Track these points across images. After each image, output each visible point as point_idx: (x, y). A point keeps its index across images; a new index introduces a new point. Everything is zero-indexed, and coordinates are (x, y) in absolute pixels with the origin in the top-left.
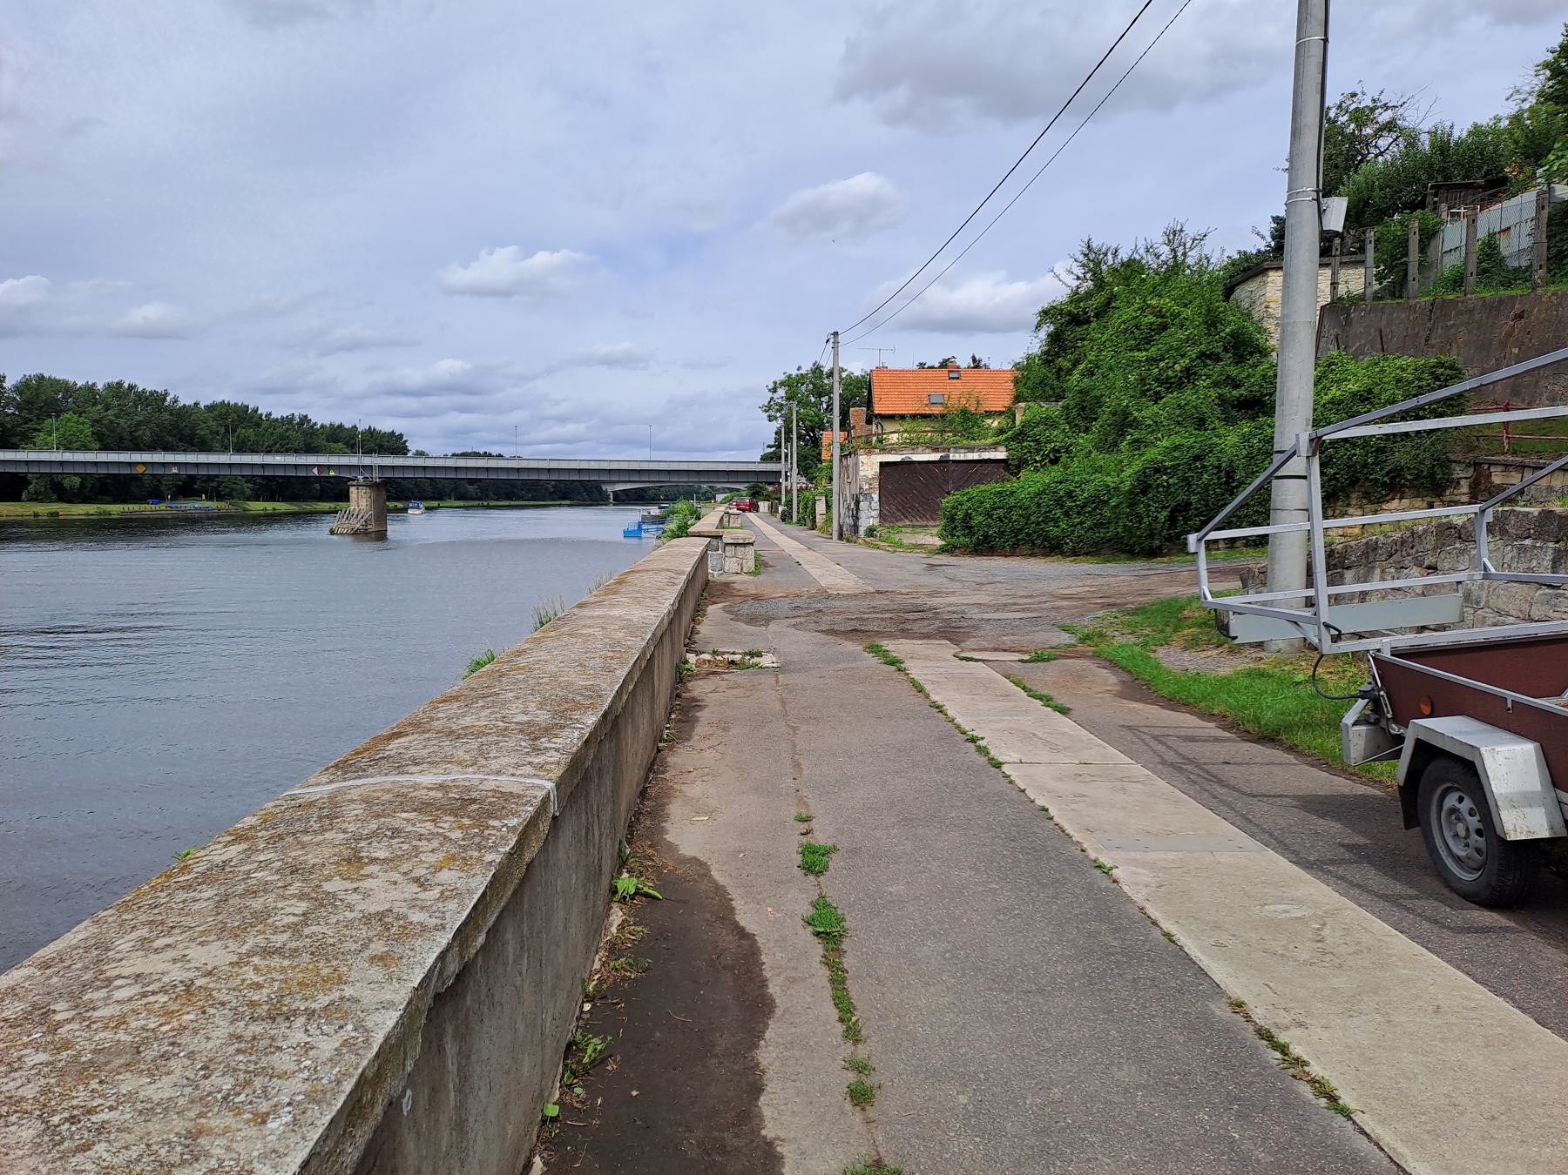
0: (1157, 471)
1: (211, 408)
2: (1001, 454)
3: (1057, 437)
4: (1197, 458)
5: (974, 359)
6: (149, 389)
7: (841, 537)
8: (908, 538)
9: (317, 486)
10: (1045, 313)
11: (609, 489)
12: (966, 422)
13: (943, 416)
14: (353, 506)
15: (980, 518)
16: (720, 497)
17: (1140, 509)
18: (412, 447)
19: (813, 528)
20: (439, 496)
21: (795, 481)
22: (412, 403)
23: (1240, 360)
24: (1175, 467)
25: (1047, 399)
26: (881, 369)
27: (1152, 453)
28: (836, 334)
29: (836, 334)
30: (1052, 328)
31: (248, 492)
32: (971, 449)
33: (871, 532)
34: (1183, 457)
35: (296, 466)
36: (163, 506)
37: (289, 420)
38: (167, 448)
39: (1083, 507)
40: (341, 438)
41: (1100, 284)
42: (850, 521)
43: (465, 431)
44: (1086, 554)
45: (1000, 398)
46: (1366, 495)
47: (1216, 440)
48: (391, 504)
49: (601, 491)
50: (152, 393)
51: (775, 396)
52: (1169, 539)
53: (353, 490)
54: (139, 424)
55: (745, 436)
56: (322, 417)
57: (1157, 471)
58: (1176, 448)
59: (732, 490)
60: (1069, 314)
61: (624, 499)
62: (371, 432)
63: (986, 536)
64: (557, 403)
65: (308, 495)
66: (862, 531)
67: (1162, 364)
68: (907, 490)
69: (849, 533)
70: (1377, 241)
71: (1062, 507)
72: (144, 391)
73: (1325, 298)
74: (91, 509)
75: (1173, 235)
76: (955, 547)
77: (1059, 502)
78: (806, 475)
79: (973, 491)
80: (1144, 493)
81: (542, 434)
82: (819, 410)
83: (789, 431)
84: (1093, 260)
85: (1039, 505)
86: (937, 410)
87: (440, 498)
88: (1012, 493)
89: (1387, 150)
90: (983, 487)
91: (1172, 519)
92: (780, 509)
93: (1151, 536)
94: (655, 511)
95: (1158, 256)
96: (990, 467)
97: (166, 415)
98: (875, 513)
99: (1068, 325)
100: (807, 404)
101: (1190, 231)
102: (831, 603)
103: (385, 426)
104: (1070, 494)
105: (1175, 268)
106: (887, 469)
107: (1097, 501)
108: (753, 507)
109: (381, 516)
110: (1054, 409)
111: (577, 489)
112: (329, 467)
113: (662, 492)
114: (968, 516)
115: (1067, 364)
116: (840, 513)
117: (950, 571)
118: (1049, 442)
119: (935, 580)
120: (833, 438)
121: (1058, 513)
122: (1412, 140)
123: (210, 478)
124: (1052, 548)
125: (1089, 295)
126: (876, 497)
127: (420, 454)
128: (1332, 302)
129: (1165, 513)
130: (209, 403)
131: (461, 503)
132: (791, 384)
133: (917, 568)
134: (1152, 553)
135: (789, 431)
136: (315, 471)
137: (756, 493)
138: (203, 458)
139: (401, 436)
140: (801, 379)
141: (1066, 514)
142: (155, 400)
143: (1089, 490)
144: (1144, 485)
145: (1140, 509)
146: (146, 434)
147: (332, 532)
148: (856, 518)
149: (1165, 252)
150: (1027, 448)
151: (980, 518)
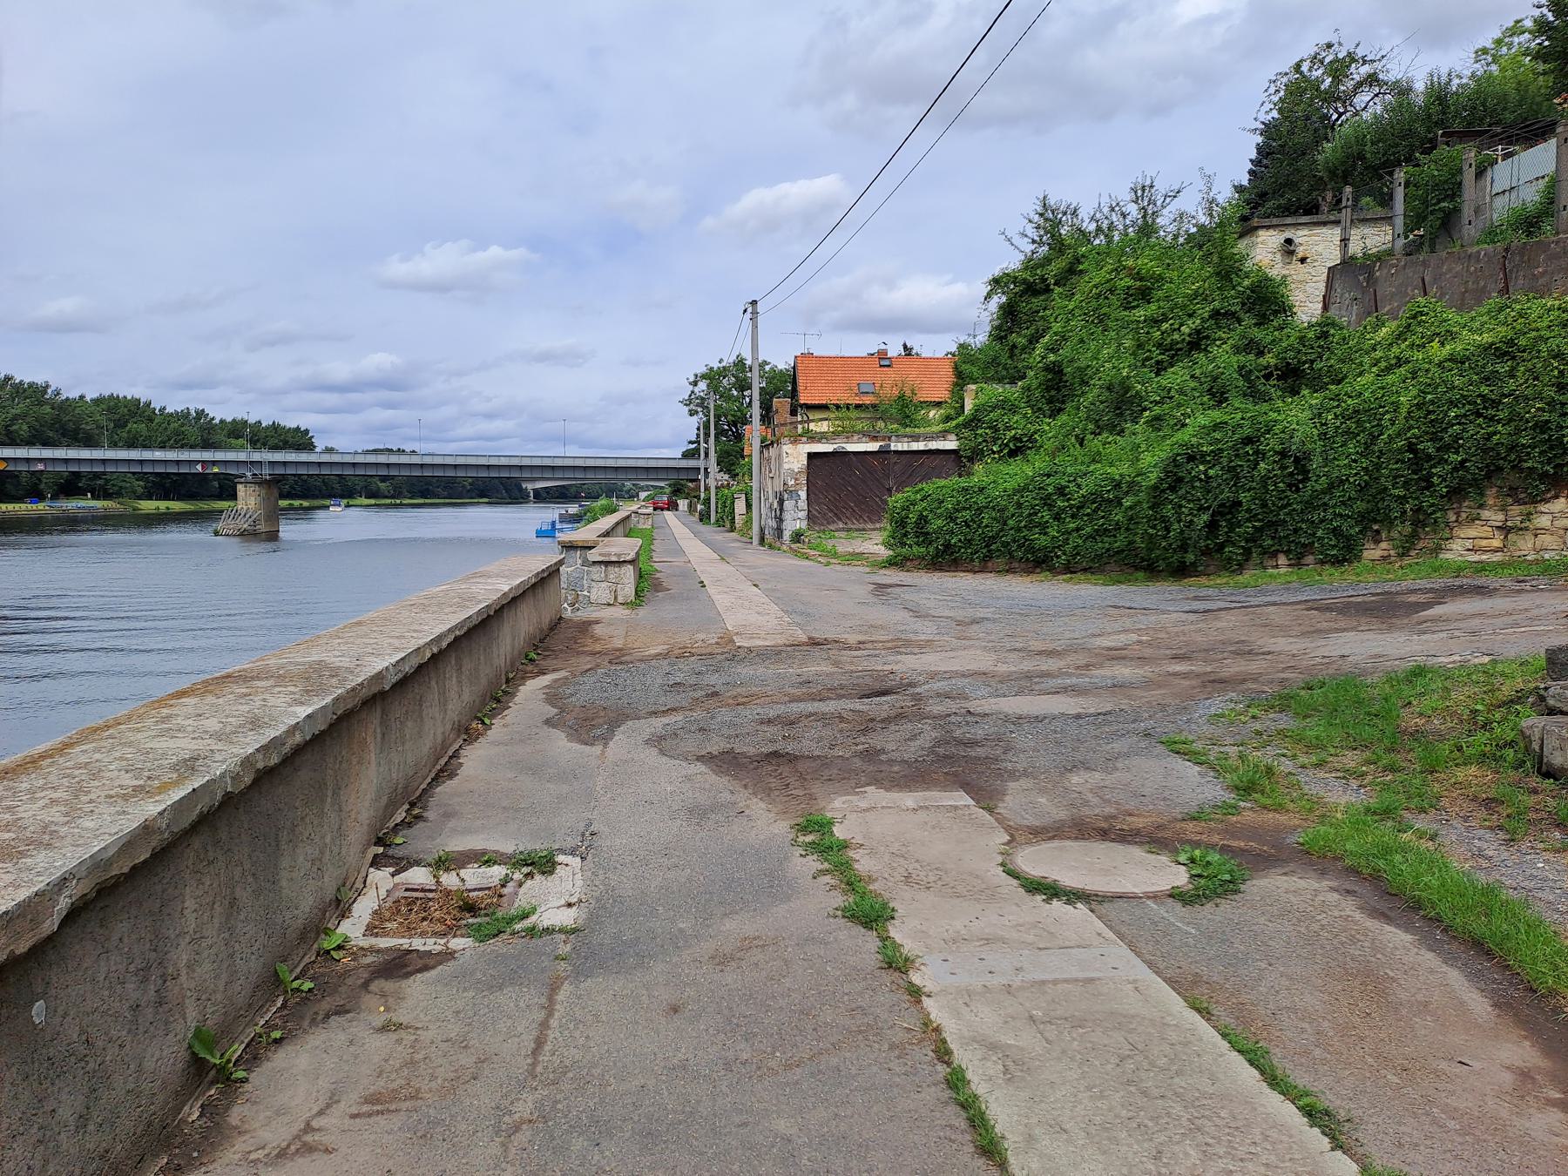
0: (1191, 458)
1: (97, 401)
2: (951, 444)
3: (1018, 424)
4: (1248, 441)
5: (905, 346)
6: (27, 380)
7: (762, 541)
8: (844, 545)
9: (216, 484)
10: (996, 281)
11: (529, 486)
12: (905, 411)
13: (874, 406)
14: (240, 504)
15: (939, 522)
16: (643, 495)
17: (1168, 511)
18: (320, 444)
19: (732, 530)
21: (716, 477)
22: (332, 399)
23: (1262, 321)
24: (1217, 454)
25: (1000, 380)
26: (808, 356)
27: (1183, 436)
28: (754, 303)
29: (754, 303)
30: (1004, 299)
31: (140, 490)
32: (916, 438)
33: (797, 537)
34: (1226, 439)
35: (178, 462)
36: (41, 506)
37: (185, 415)
38: (46, 443)
39: (1079, 508)
40: (237, 431)
41: (1058, 246)
42: (773, 523)
43: (389, 427)
44: (1085, 570)
45: (938, 388)
46: (1512, 492)
47: (1274, 415)
48: (283, 503)
49: (521, 489)
50: (31, 385)
51: (696, 390)
52: (1206, 552)
53: (239, 487)
54: (15, 418)
55: (668, 433)
56: (221, 412)
57: (1191, 458)
58: (1217, 427)
59: (655, 487)
60: (1025, 281)
61: (542, 497)
62: (275, 427)
63: (947, 546)
64: (489, 400)
65: (194, 493)
66: (787, 535)
67: (1165, 326)
68: (841, 487)
69: (770, 539)
70: (1407, 184)
71: (1051, 506)
72: (21, 383)
73: (1334, 258)
75: (1142, 192)
76: (906, 559)
77: (1047, 502)
78: (729, 471)
79: (928, 487)
80: (1173, 489)
81: (467, 429)
82: (740, 406)
83: (707, 427)
84: (1050, 220)
85: (1019, 505)
86: (867, 400)
88: (982, 490)
89: (1369, 106)
90: (942, 482)
91: (1212, 526)
92: (699, 507)
93: (1184, 548)
94: (573, 509)
95: (1124, 216)
96: (938, 460)
97: (47, 409)
98: (803, 514)
99: (1023, 297)
100: (729, 398)
101: (1161, 187)
102: (745, 671)
103: (290, 422)
104: (1061, 491)
105: (1147, 229)
106: (817, 462)
107: (1101, 501)
108: (672, 506)
109: (274, 515)
110: (1013, 391)
111: (496, 485)
112: (214, 463)
113: (579, 487)
114: (922, 519)
115: (1022, 341)
116: (762, 515)
117: (908, 595)
118: (1009, 428)
119: (890, 617)
120: (754, 432)
121: (1046, 515)
122: (1402, 90)
123: (97, 476)
124: (1038, 562)
125: (1047, 261)
126: (803, 494)
127: (329, 450)
128: (1344, 262)
129: (1205, 517)
130: (95, 396)
131: (373, 501)
133: (863, 591)
134: (1181, 571)
135: (707, 427)
136: (199, 467)
137: (678, 491)
138: (85, 454)
139: (307, 431)
140: (723, 372)
141: (1057, 518)
142: (35, 393)
143: (1088, 486)
144: (1173, 479)
145: (1168, 511)
146: (23, 428)
147: (216, 533)
148: (780, 520)
149: (1133, 210)
150: (985, 438)
151: (939, 522)
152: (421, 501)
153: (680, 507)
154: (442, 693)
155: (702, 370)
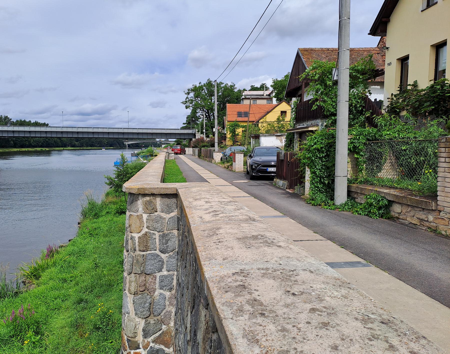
11: (126, 143)
16: (163, 146)
20: (65, 146)
49: (124, 144)
51: (189, 96)
74: (18, 149)
87: (65, 147)
108: (182, 152)
131: (73, 148)
132: (197, 90)
140: (201, 88)
152: (90, 148)
153: (187, 153)
154: (434, 119)
155: (191, 86)
